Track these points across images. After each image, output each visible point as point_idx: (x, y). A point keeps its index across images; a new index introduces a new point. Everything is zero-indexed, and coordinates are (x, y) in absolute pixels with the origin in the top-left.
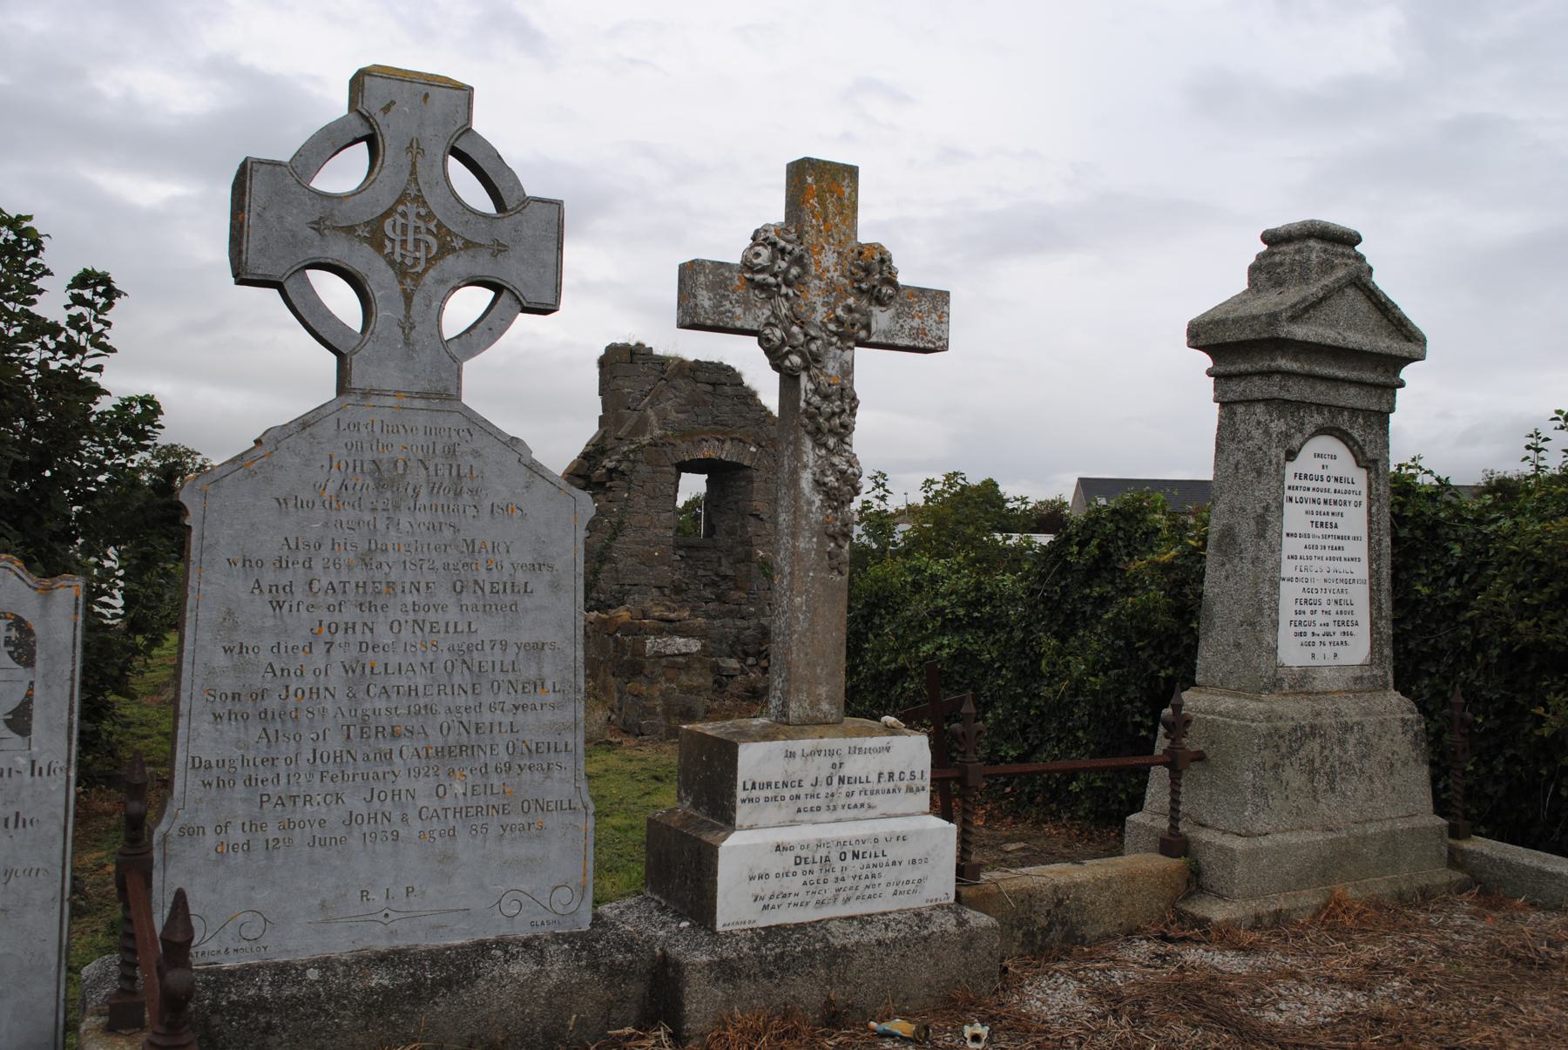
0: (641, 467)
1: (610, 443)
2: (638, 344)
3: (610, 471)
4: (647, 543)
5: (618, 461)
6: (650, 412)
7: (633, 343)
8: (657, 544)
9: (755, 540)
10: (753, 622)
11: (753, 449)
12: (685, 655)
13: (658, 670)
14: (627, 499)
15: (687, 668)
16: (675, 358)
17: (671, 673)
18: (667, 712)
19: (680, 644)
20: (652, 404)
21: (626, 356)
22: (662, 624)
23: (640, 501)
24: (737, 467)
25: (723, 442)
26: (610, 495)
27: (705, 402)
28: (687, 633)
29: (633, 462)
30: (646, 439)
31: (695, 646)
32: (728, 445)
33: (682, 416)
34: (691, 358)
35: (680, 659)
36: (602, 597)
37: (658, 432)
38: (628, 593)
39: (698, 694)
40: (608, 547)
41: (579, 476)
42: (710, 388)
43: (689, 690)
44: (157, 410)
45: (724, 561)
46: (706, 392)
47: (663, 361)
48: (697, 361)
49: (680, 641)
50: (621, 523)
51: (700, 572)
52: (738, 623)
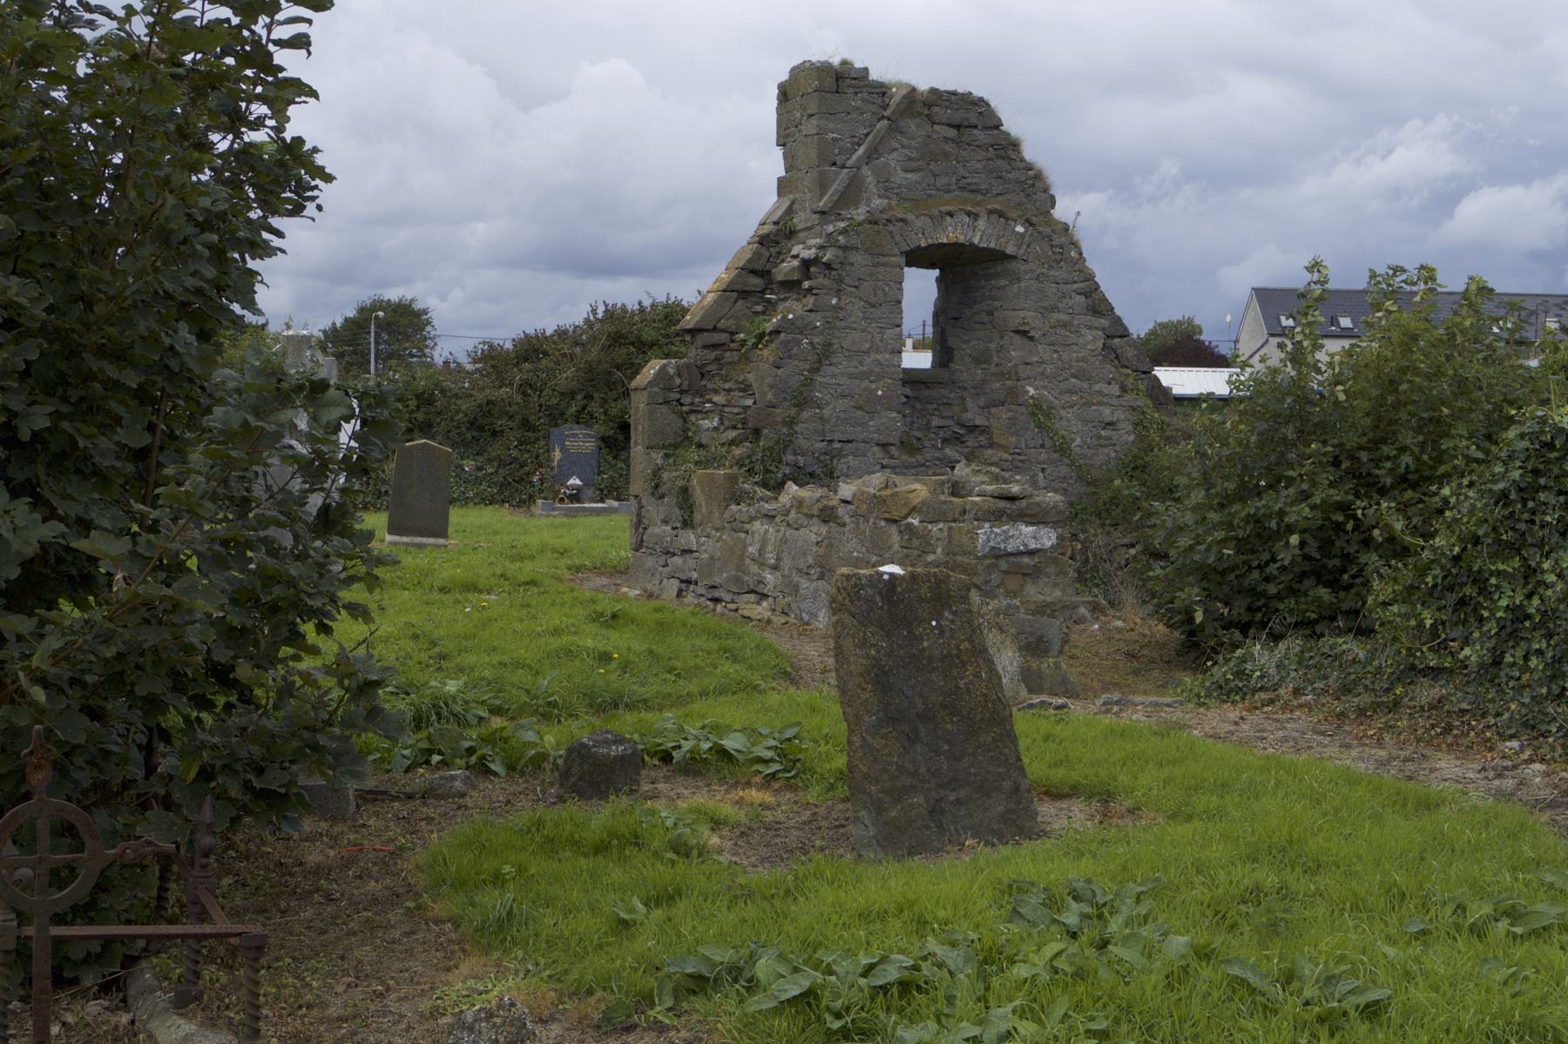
0: (857, 258)
1: (799, 221)
2: (844, 63)
3: (806, 264)
4: (864, 376)
5: (821, 247)
6: (866, 171)
7: (836, 61)
8: (880, 377)
9: (1024, 371)
11: (1020, 229)
13: (995, 577)
14: (838, 308)
15: (1035, 573)
16: (900, 85)
17: (1013, 582)
19: (1026, 535)
20: (869, 158)
21: (829, 82)
22: (1002, 504)
24: (996, 257)
25: (976, 216)
26: (810, 300)
27: (946, 155)
28: (1036, 517)
29: (845, 248)
30: (860, 213)
31: (1047, 538)
32: (981, 224)
35: (1026, 560)
36: (801, 460)
37: (878, 202)
38: (840, 454)
40: (809, 382)
41: (754, 272)
42: (952, 133)
43: (1041, 610)
44: (958, 130)
45: (969, 403)
47: (882, 90)
48: (933, 91)
51: (936, 422)
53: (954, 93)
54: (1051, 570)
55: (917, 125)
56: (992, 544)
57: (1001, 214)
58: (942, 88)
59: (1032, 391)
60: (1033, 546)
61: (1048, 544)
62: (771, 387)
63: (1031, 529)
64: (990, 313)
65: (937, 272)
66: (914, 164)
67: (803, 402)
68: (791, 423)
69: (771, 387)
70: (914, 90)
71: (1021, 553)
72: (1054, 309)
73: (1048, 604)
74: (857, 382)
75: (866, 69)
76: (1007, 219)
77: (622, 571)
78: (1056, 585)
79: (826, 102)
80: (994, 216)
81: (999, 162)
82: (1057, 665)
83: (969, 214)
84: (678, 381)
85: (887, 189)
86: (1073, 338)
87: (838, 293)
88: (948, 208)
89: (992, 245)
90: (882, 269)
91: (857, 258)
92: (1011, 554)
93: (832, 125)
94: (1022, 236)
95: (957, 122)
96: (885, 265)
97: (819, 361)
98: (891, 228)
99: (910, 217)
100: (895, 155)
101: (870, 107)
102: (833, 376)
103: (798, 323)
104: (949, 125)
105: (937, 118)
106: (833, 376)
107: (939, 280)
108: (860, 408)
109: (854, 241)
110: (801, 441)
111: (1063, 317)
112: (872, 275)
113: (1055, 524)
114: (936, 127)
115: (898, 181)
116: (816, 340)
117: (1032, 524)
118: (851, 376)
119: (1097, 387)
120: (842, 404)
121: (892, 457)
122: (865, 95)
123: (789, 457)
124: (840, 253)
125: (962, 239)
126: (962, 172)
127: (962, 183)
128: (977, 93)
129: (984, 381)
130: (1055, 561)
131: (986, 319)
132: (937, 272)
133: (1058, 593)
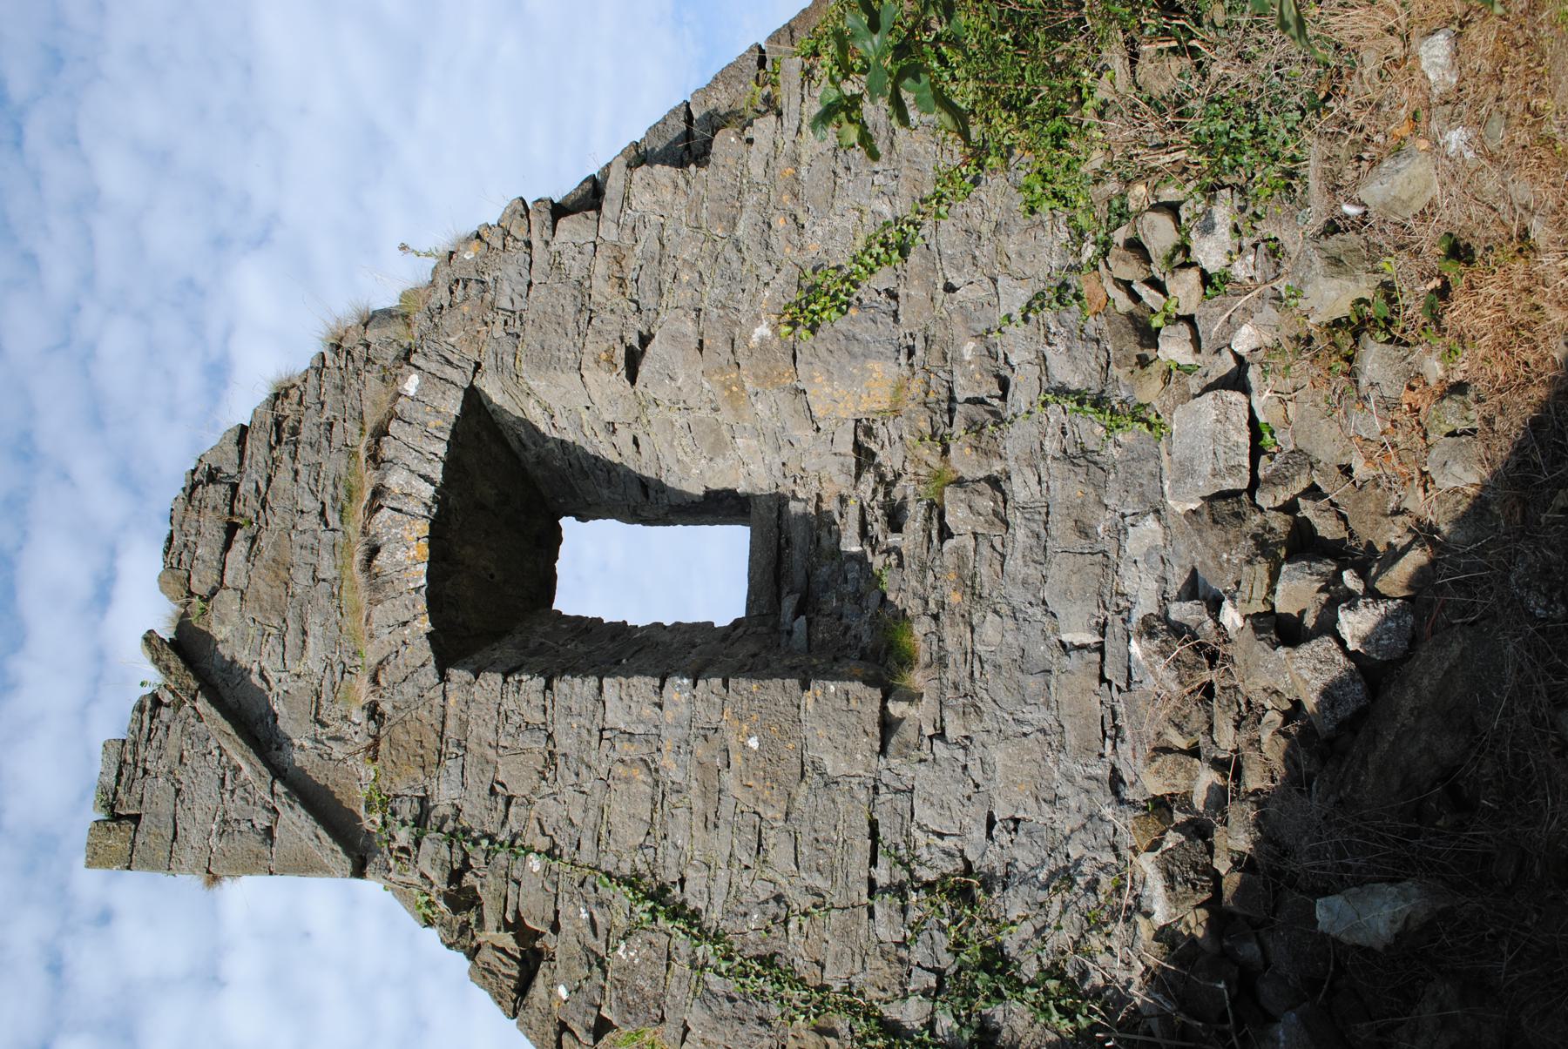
10: (1019, 349)
11: (412, 384)
41: (523, 987)
42: (240, 546)
52: (1022, 396)
57: (381, 432)
59: (763, 330)
64: (611, 428)
65: (567, 523)
66: (293, 626)
72: (582, 287)
77: (1211, 92)
83: (373, 509)
86: (648, 236)
89: (441, 449)
96: (464, 724)
104: (227, 547)
105: (212, 577)
107: (582, 518)
111: (601, 267)
114: (228, 580)
119: (757, 171)
129: (758, 433)
131: (624, 437)
132: (567, 523)
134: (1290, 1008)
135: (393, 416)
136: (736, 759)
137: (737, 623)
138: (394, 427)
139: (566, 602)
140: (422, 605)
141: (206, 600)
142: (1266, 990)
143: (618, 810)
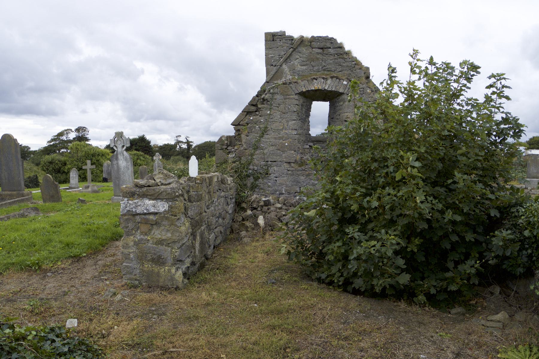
11: (345, 83)
12: (155, 214)
14: (270, 114)
15: (157, 224)
17: (144, 228)
18: (141, 258)
19: (148, 205)
20: (286, 61)
23: (277, 115)
25: (327, 79)
27: (318, 59)
28: (156, 197)
29: (273, 94)
30: (280, 82)
31: (162, 207)
32: (329, 81)
33: (304, 67)
34: (310, 36)
35: (151, 217)
36: (256, 168)
38: (271, 166)
39: (168, 245)
40: (259, 141)
43: (160, 242)
44: (326, 50)
46: (318, 53)
47: (291, 38)
48: (313, 37)
49: (149, 203)
50: (266, 128)
53: (320, 37)
54: (165, 223)
55: (306, 50)
56: (128, 209)
58: (315, 36)
60: (152, 210)
61: (162, 210)
62: (245, 143)
63: (151, 202)
64: (339, 115)
66: (305, 63)
67: (256, 147)
68: (252, 155)
69: (245, 143)
70: (303, 37)
71: (145, 214)
73: (163, 240)
74: (278, 141)
75: (285, 32)
76: (340, 80)
78: (168, 231)
79: (279, 45)
80: (334, 79)
81: (339, 60)
82: (169, 271)
83: (323, 78)
84: (226, 142)
85: (294, 73)
87: (270, 109)
88: (315, 77)
89: (333, 89)
90: (287, 100)
91: (278, 97)
92: (140, 214)
93: (271, 52)
94: (346, 85)
95: (321, 47)
96: (288, 99)
97: (263, 134)
98: (291, 85)
99: (300, 81)
100: (297, 60)
101: (286, 45)
102: (268, 139)
103: (254, 120)
106: (268, 139)
108: (279, 150)
109: (276, 90)
110: (256, 161)
112: (283, 102)
113: (167, 200)
114: (314, 49)
115: (299, 69)
116: (261, 126)
117: (153, 200)
118: (275, 138)
120: (271, 148)
121: (292, 167)
122: (284, 41)
123: (251, 167)
124: (270, 95)
125: (320, 88)
126: (324, 64)
127: (324, 68)
128: (330, 36)
130: (167, 218)
132: (328, 103)
133: (169, 235)
134: (443, 205)
135: (340, 80)
136: (284, 142)
137: (310, 135)
138: (338, 80)
139: (328, 103)
140: (307, 89)
141: (310, 45)
142: (255, 211)
143: (277, 124)
